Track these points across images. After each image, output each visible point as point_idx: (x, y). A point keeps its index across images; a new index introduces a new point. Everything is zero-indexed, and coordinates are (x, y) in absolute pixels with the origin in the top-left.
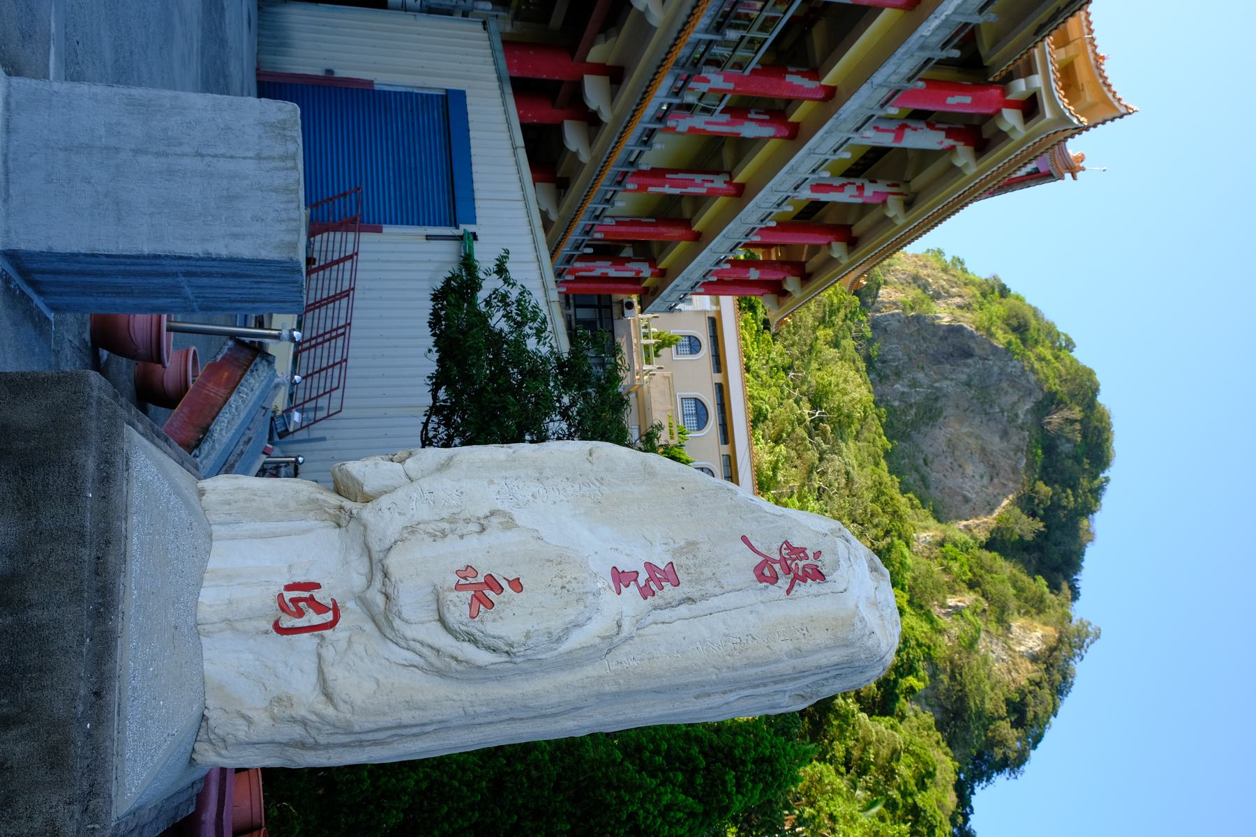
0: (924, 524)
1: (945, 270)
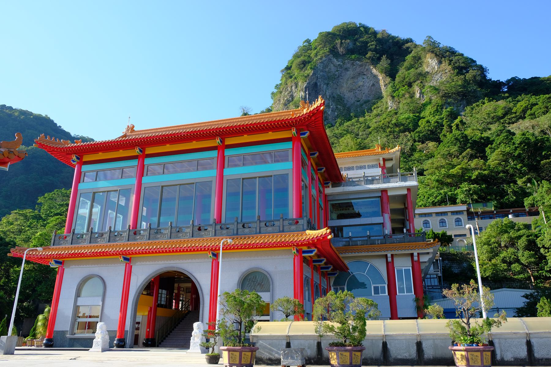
0: (385, 104)
1: (281, 92)
